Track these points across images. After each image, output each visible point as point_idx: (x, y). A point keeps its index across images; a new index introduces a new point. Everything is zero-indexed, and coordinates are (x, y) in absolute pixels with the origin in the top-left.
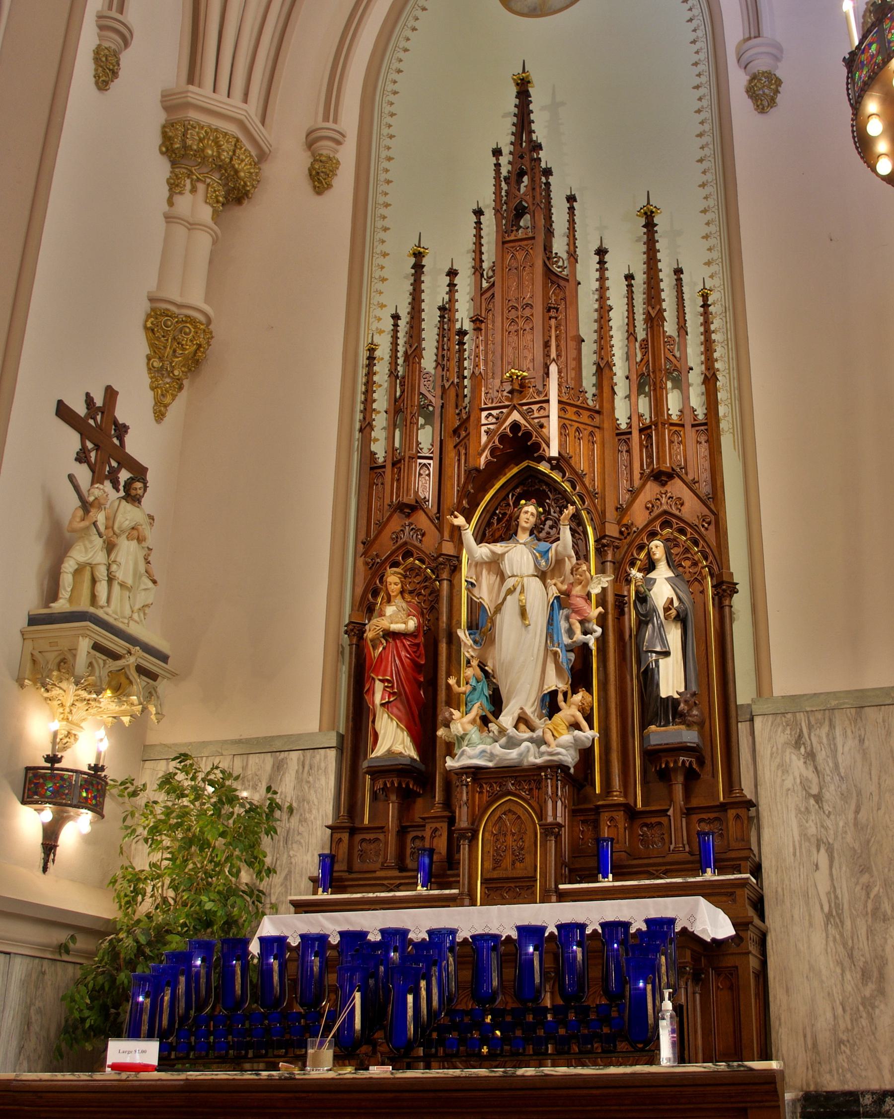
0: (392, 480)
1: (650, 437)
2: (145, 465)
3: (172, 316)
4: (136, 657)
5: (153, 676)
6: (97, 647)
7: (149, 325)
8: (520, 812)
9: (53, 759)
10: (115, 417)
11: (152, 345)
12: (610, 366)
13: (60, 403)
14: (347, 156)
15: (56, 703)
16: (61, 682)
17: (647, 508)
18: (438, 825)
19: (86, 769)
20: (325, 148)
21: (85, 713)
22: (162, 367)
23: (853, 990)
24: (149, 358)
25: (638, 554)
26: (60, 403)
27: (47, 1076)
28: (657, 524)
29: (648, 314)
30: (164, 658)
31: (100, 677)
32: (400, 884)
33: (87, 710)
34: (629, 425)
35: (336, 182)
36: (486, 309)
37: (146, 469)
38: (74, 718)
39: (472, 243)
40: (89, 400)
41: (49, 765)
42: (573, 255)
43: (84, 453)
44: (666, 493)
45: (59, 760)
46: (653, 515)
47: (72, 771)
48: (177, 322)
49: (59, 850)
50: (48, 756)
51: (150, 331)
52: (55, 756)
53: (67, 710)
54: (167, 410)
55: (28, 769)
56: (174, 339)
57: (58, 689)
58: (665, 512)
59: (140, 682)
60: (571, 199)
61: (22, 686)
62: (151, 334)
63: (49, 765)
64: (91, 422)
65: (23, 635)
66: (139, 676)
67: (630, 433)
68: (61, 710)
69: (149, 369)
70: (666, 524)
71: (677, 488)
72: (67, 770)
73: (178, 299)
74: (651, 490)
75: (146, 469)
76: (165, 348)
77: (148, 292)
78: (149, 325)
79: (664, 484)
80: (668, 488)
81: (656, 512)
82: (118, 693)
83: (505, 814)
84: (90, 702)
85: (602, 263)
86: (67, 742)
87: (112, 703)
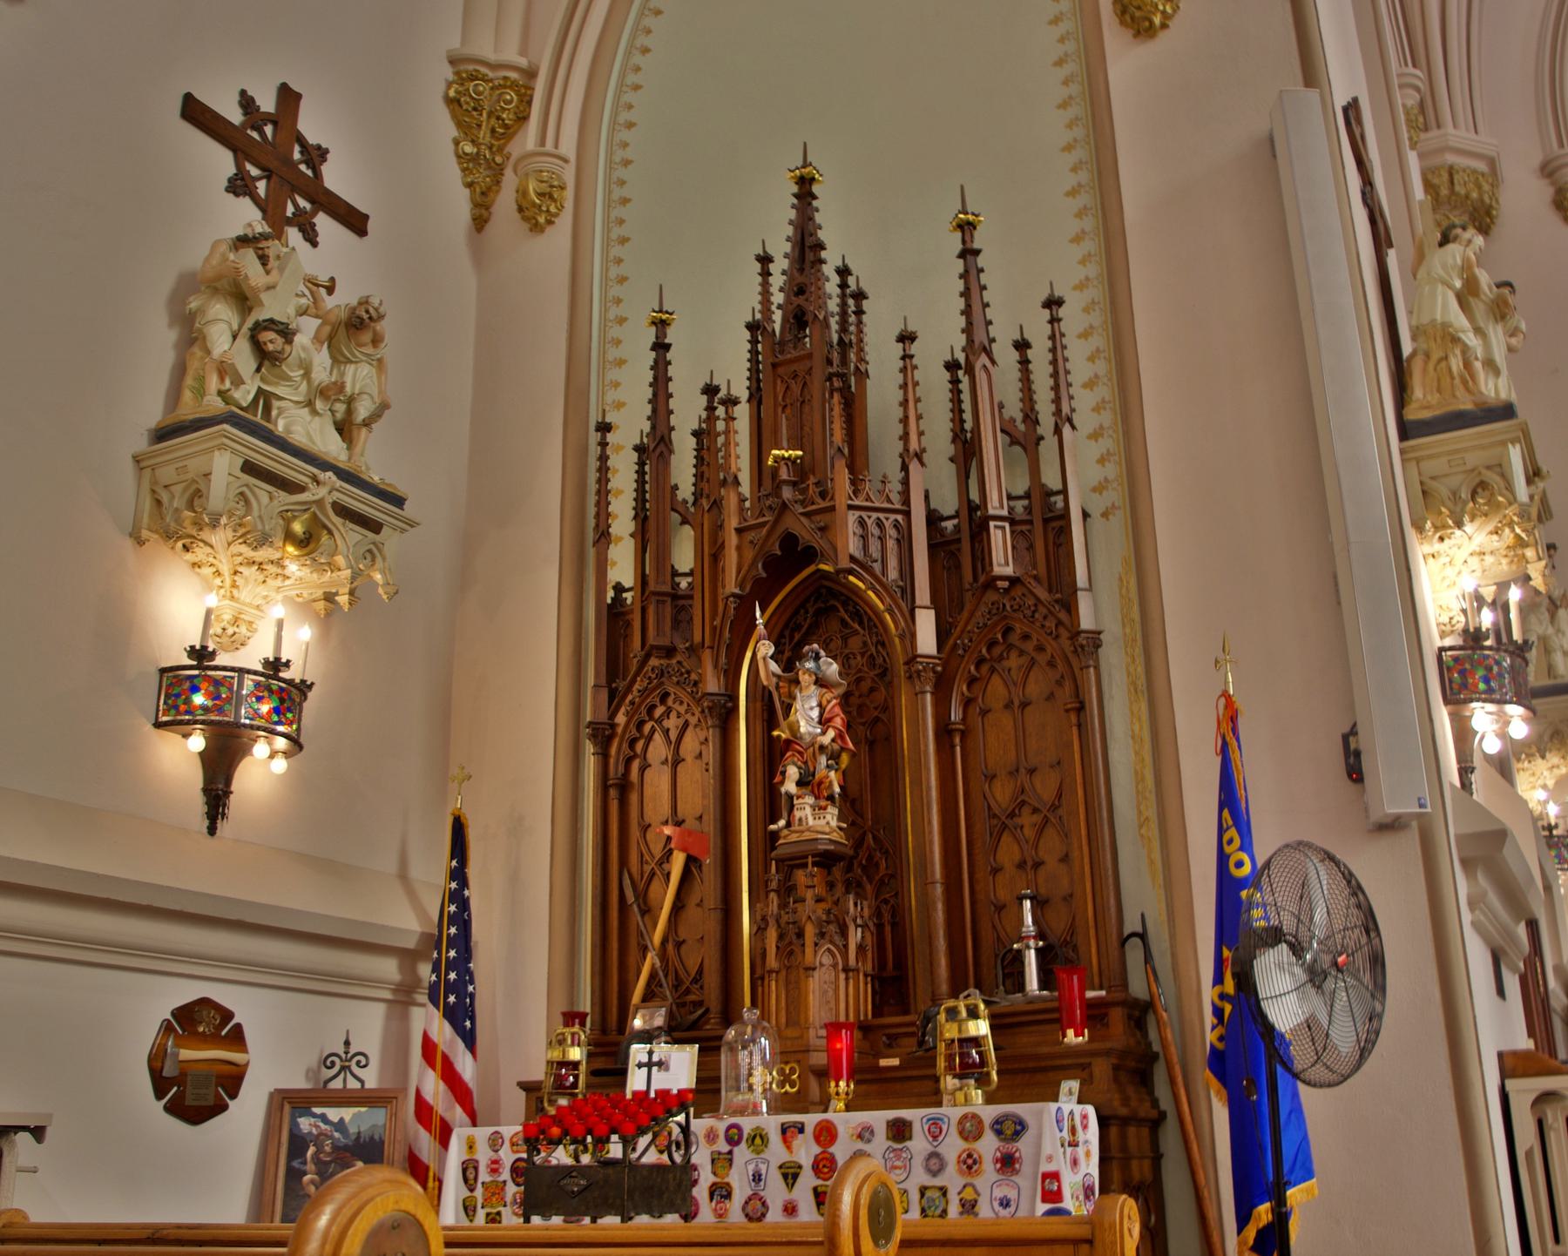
2: (364, 211)
3: (485, 79)
4: (328, 489)
5: (374, 526)
6: (249, 468)
7: (452, 93)
9: (201, 655)
10: (298, 131)
11: (459, 124)
13: (189, 99)
15: (207, 571)
16: (201, 529)
19: (259, 668)
21: (262, 586)
22: (478, 154)
24: (456, 143)
26: (189, 99)
30: (399, 501)
31: (260, 517)
33: (264, 582)
36: (1054, 543)
37: (366, 217)
38: (245, 594)
39: (1017, 390)
40: (247, 102)
43: (242, 179)
47: (233, 669)
48: (492, 88)
49: (233, 800)
50: (192, 647)
51: (456, 104)
52: (204, 648)
53: (228, 582)
54: (490, 213)
55: (163, 671)
56: (490, 114)
57: (201, 544)
59: (350, 536)
61: (140, 542)
62: (457, 107)
64: (255, 135)
65: (138, 462)
66: (344, 524)
68: (218, 581)
69: (458, 157)
72: (224, 668)
73: (491, 56)
75: (366, 217)
76: (479, 126)
77: (448, 51)
78: (452, 93)
82: (308, 549)
84: (265, 567)
86: (235, 633)
87: (304, 568)
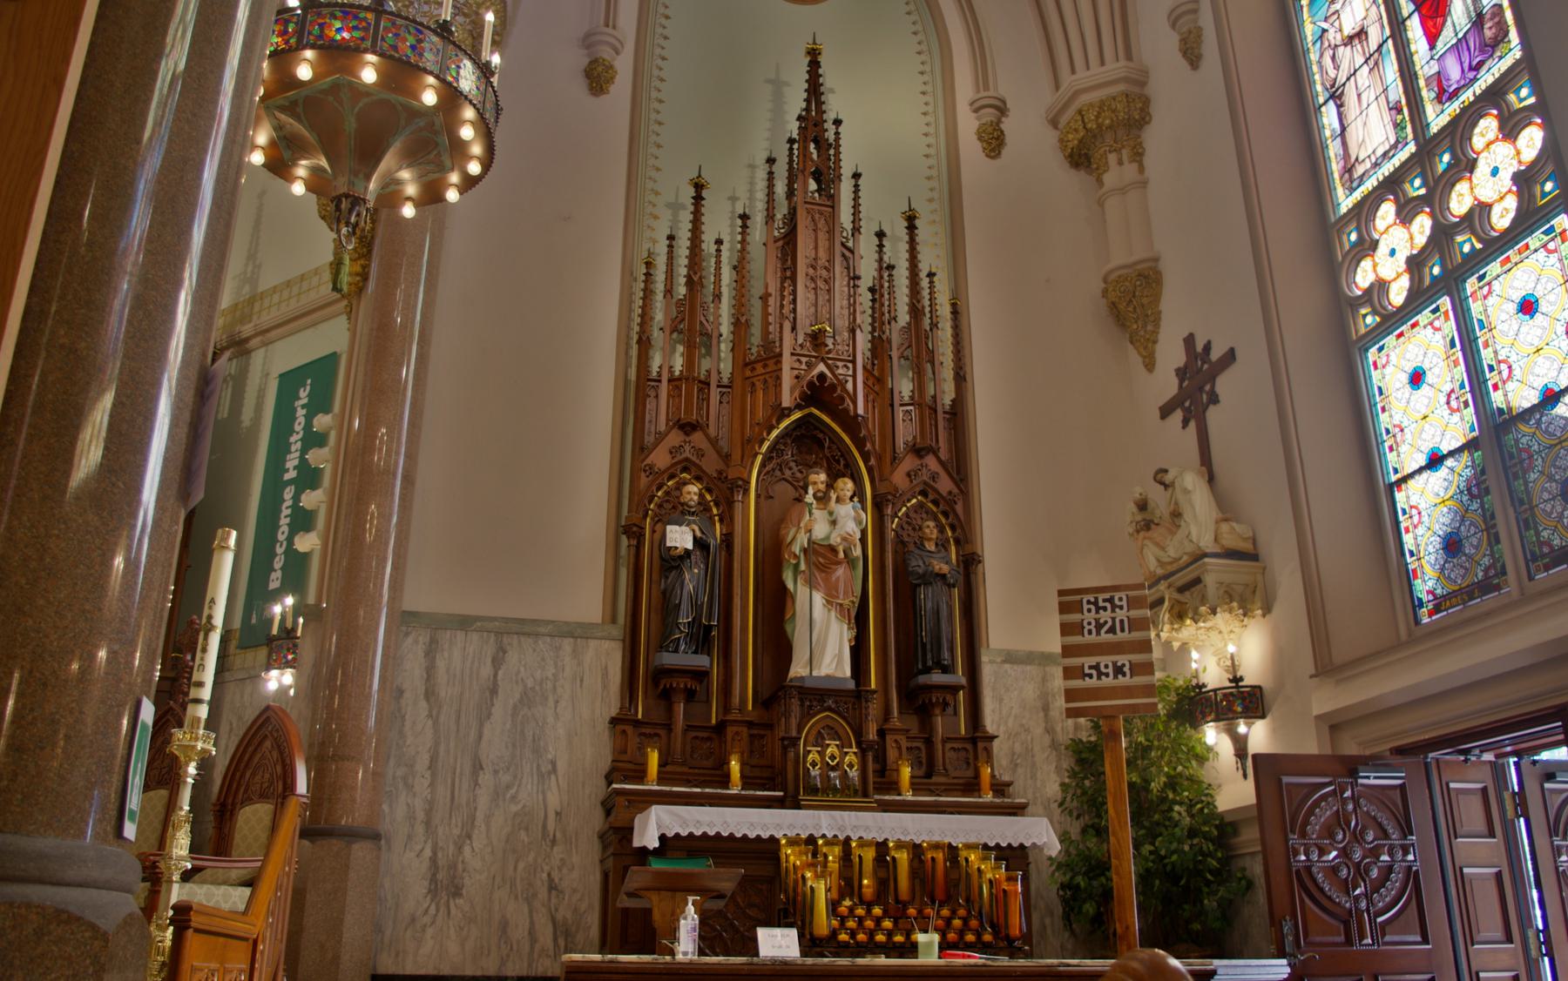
0: (931, 424)
1: (679, 388)
8: (837, 727)
12: (748, 324)
14: (623, 65)
17: (671, 453)
18: (740, 729)
20: (605, 53)
23: (863, 540)
25: (657, 491)
27: (597, 957)
28: (679, 467)
29: (689, 277)
32: (704, 781)
34: (659, 374)
35: (613, 88)
41: (1234, 685)
42: (856, 230)
44: (690, 442)
45: (1241, 679)
46: (676, 460)
58: (687, 459)
60: (856, 176)
63: (1234, 685)
67: (660, 381)
70: (685, 470)
71: (697, 437)
74: (675, 438)
79: (687, 434)
80: (691, 438)
81: (679, 458)
83: (823, 728)
85: (744, 226)
